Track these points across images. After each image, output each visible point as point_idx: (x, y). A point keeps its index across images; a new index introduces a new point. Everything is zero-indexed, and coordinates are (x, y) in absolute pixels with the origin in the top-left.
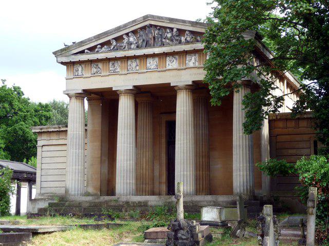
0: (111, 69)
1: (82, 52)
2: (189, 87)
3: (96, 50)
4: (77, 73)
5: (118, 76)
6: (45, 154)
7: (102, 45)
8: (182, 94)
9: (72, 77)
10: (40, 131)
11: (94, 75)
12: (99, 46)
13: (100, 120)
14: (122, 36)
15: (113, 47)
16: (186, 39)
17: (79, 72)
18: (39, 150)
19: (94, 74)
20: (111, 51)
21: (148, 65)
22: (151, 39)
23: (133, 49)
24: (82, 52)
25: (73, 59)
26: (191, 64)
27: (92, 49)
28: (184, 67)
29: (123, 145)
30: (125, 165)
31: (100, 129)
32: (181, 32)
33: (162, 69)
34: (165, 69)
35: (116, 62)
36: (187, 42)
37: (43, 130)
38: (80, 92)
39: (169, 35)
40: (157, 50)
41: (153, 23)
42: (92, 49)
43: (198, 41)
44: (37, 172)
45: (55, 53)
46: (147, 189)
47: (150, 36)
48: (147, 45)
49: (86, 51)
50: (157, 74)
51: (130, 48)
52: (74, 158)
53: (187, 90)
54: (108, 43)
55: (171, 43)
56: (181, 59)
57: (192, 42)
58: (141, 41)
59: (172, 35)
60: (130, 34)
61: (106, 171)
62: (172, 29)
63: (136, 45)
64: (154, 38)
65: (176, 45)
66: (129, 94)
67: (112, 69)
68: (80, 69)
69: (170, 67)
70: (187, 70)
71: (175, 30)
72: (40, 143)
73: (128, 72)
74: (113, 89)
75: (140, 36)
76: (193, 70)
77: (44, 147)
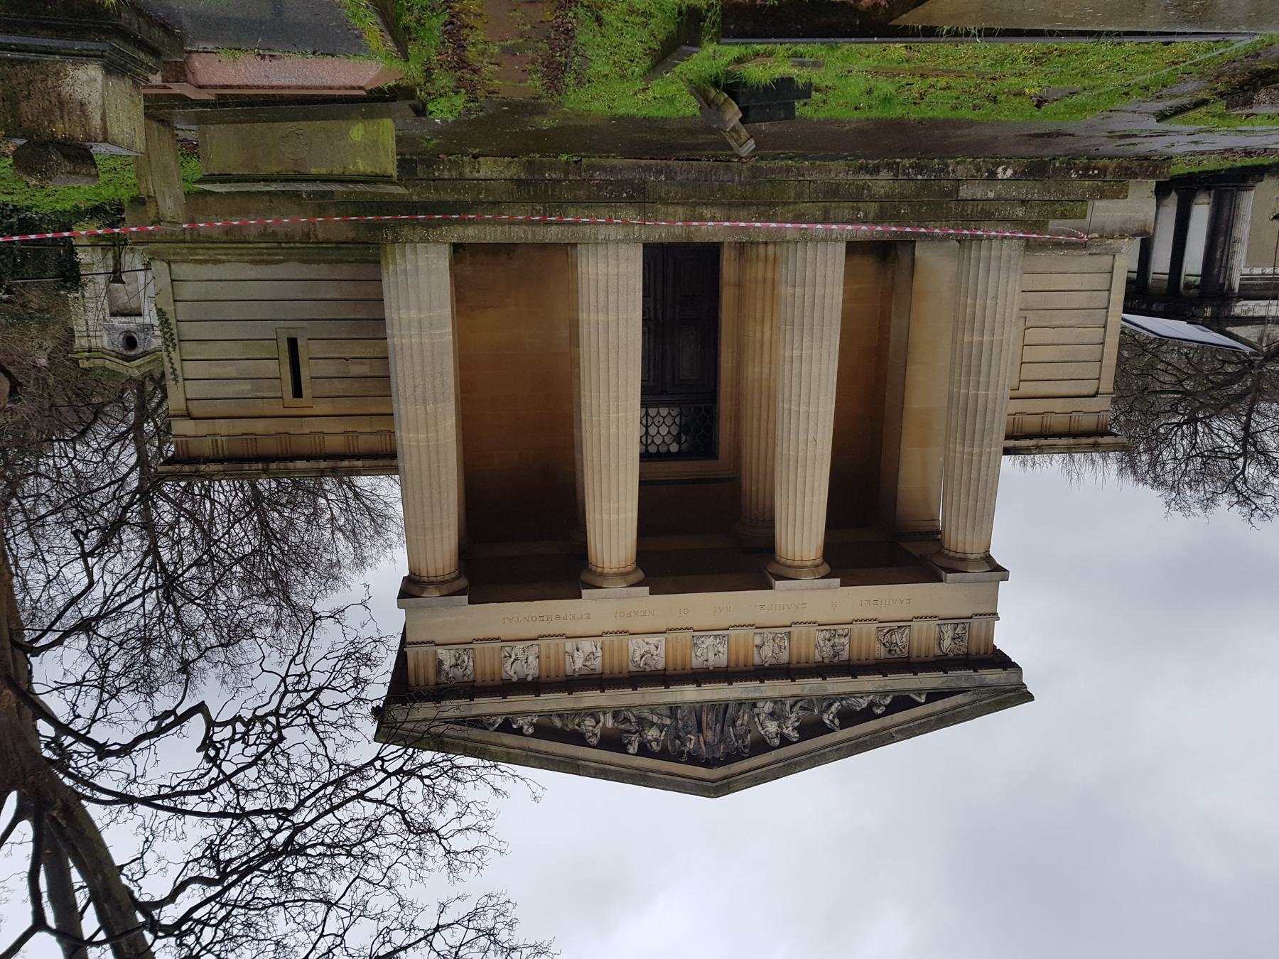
0: (846, 640)
1: (933, 696)
2: (598, 582)
3: (888, 700)
4: (959, 630)
5: (821, 620)
6: (1092, 370)
7: (867, 714)
8: (623, 555)
9: (975, 622)
10: (1100, 440)
11: (902, 624)
12: (879, 712)
13: (903, 473)
14: (600, 746)
15: (833, 709)
16: (598, 722)
17: (951, 634)
18: (1107, 384)
19: (899, 627)
20: (840, 697)
21: (723, 649)
22: (708, 727)
23: (765, 699)
24: (933, 696)
25: (967, 678)
26: (587, 645)
27: (902, 702)
28: (606, 639)
29: (812, 409)
30: (806, 343)
31: (902, 446)
32: (613, 742)
33: (680, 635)
34: (670, 635)
35: (826, 661)
36: (593, 713)
37: (1091, 440)
38: (950, 576)
39: (652, 733)
40: (689, 694)
42: (902, 702)
43: (560, 716)
44: (1116, 314)
45: (1030, 697)
46: (761, 265)
47: (709, 735)
48: (722, 711)
49: (923, 699)
51: (775, 702)
52: (984, 369)
53: (599, 570)
54: (849, 718)
55: (646, 714)
56: (616, 662)
57: (577, 713)
58: (739, 722)
59: (640, 732)
60: (777, 741)
61: (894, 321)
62: (644, 751)
63: (756, 711)
64: (700, 729)
65: (628, 708)
66: (789, 562)
67: (842, 640)
68: (947, 642)
69: (653, 640)
70: (600, 633)
71: (633, 749)
72: (1103, 403)
73: (788, 630)
74: (838, 580)
75: (743, 737)
77: (1092, 392)
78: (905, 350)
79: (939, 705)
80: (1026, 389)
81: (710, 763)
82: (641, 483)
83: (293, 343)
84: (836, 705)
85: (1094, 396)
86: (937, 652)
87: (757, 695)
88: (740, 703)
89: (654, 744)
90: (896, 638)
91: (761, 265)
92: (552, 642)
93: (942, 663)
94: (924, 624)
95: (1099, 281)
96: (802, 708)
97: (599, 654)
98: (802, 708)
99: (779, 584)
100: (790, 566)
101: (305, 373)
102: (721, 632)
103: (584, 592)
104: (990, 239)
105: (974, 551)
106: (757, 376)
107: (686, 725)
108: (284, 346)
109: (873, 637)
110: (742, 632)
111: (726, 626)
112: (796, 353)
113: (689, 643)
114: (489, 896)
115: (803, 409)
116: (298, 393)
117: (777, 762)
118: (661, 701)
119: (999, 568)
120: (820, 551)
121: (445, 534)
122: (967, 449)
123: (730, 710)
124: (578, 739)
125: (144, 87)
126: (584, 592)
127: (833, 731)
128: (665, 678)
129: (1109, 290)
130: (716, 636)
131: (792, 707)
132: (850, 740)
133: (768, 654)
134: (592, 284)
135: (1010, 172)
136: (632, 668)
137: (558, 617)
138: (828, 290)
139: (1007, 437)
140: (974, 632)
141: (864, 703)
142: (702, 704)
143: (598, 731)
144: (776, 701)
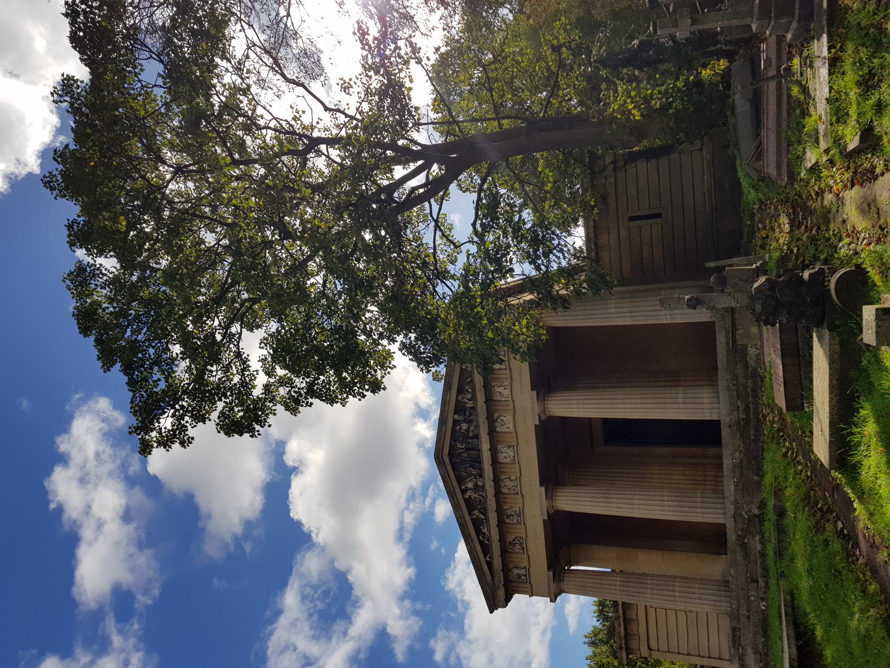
0: (515, 521)
1: (490, 564)
3: (486, 542)
7: (479, 532)
9: (528, 585)
15: (481, 515)
17: (521, 573)
19: (523, 548)
20: (487, 518)
21: (508, 460)
23: (484, 482)
24: (490, 564)
26: (507, 392)
27: (486, 549)
32: (460, 408)
33: (514, 439)
36: (474, 398)
37: (624, 646)
40: (485, 445)
41: (446, 451)
42: (486, 549)
43: (472, 381)
46: (714, 474)
48: (477, 461)
49: (487, 559)
50: (520, 447)
54: (476, 523)
57: (474, 389)
60: (463, 487)
62: (456, 422)
63: (478, 477)
64: (467, 449)
65: (477, 415)
68: (516, 571)
69: (511, 426)
71: (456, 417)
74: (546, 518)
76: (514, 389)
77: (652, 646)
78: (670, 549)
79: (485, 567)
80: (651, 612)
81: (450, 455)
82: (590, 419)
83: (659, 216)
84: (483, 517)
85: (649, 647)
86: (511, 566)
87: (486, 478)
88: (481, 469)
89: (459, 427)
90: (517, 546)
91: (714, 474)
92: (508, 376)
93: (506, 569)
94: (526, 560)
95: (715, 652)
96: (480, 500)
97: (503, 399)
98: (480, 500)
99: (543, 489)
100: (552, 495)
101: (643, 222)
102: (516, 460)
103: (535, 392)
104: (718, 397)
105: (564, 585)
106: (653, 472)
107: (469, 443)
108: (657, 211)
109: (517, 535)
110: (517, 470)
111: (521, 463)
112: (666, 498)
113: (510, 444)
114: (441, 19)
115: (636, 502)
116: (631, 219)
117: (453, 486)
118: (481, 431)
119: (556, 598)
120: (561, 509)
121: (562, 322)
122: (618, 583)
123: (478, 464)
124: (461, 391)
125: (780, 39)
126: (535, 392)
127: (470, 515)
128: (493, 433)
129: (709, 657)
130: (514, 457)
131: (481, 495)
132: (466, 523)
133: (507, 485)
134: (698, 395)
135: (764, 608)
136: (496, 415)
137: (521, 379)
138: (700, 515)
139: (623, 603)
140: (523, 585)
141: (485, 530)
142: (479, 450)
143: (465, 400)
144: (483, 487)
